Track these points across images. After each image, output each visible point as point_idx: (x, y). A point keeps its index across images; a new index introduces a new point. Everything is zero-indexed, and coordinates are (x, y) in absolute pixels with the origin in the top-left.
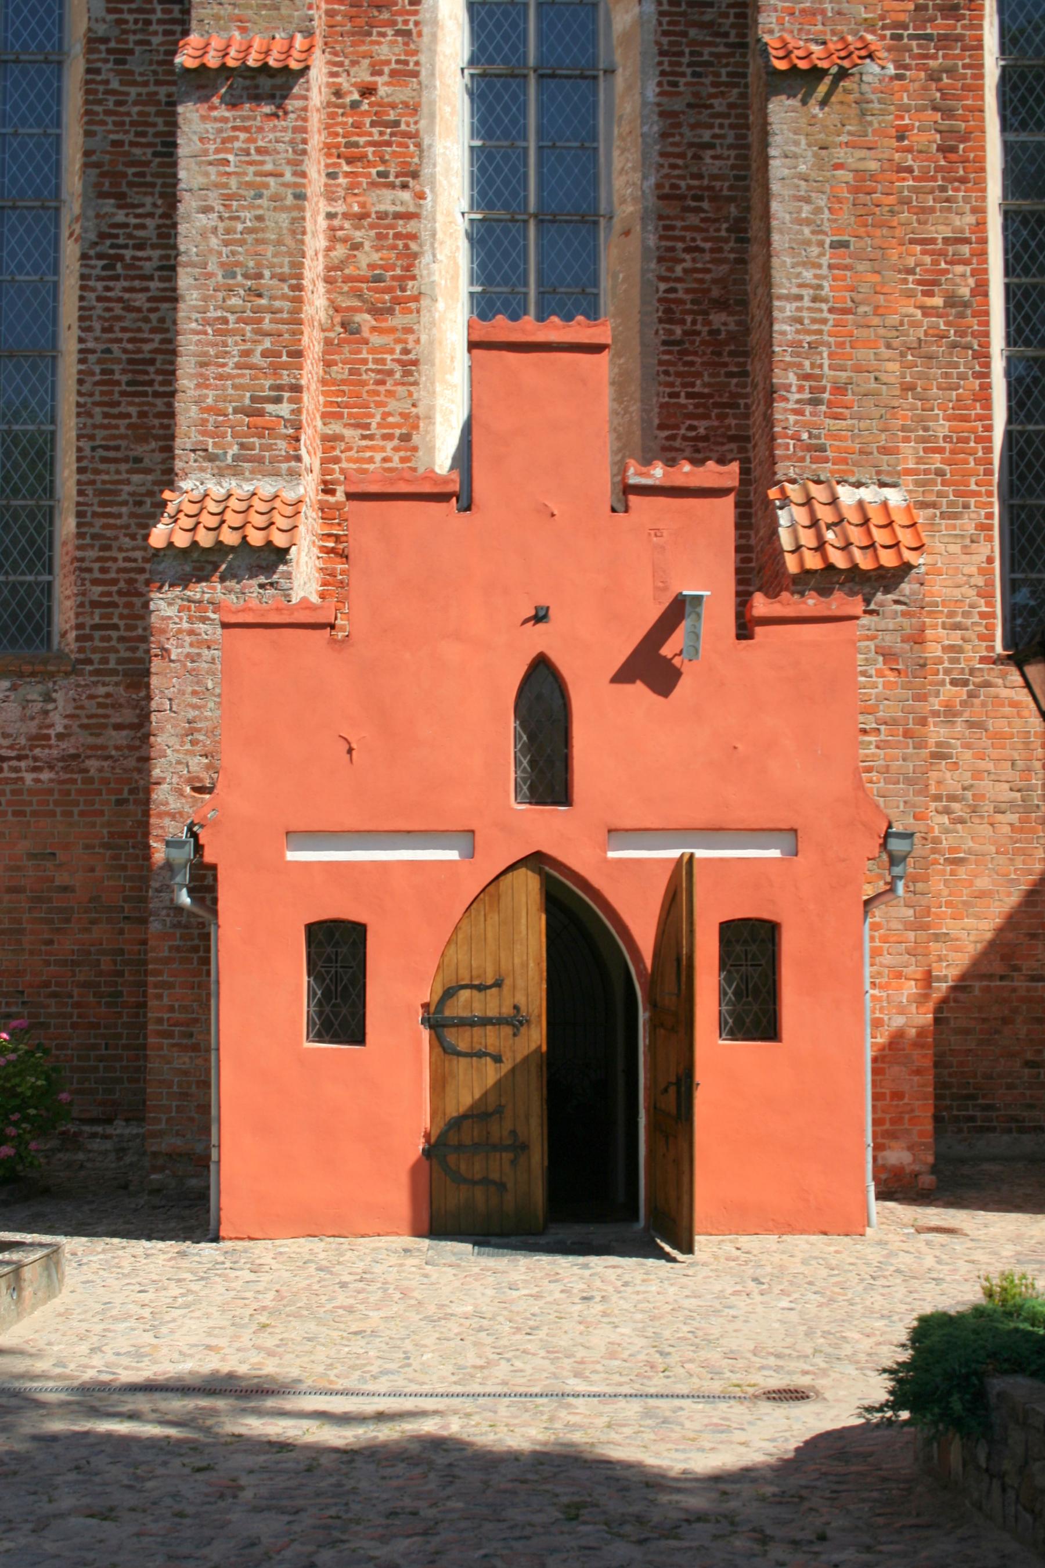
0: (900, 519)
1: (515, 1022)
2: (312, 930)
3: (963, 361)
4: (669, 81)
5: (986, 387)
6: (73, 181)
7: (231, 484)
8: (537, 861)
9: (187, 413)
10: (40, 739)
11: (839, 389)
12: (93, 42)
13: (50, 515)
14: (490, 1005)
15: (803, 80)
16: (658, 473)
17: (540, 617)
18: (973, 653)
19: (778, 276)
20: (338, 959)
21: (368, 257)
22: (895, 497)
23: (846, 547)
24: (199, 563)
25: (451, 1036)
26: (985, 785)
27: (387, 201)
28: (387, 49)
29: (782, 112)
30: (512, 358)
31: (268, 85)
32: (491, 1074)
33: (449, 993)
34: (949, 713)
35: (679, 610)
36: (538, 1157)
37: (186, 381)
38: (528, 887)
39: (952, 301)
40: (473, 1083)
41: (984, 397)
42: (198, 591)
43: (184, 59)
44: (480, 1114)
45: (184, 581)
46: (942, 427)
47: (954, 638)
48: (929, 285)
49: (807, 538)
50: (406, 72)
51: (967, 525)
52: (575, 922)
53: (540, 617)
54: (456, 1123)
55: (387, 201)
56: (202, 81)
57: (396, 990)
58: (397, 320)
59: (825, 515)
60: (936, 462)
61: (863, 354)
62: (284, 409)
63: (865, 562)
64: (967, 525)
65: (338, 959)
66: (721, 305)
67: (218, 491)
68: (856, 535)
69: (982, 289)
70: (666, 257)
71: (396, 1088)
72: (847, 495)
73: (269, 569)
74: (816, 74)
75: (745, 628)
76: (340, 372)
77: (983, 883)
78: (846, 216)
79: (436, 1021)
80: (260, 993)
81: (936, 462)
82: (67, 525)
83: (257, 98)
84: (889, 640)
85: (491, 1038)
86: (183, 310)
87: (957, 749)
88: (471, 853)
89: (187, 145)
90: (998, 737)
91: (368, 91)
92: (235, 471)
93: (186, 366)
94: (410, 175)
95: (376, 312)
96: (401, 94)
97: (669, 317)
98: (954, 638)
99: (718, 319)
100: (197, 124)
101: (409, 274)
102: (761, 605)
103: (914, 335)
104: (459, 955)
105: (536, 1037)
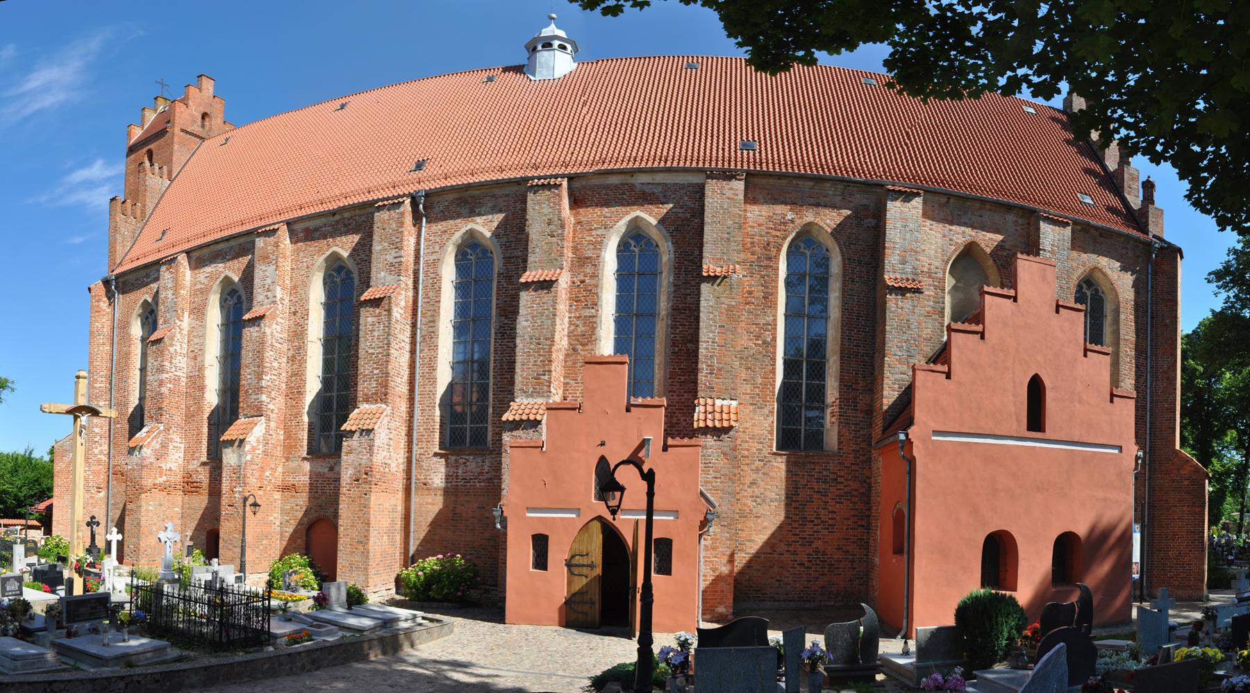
0: (732, 411)
1: (592, 566)
2: (547, 537)
3: (767, 360)
4: (677, 276)
5: (774, 369)
6: (494, 313)
7: (531, 401)
8: (600, 518)
9: (518, 379)
10: (481, 473)
11: (719, 370)
12: (499, 274)
13: (487, 407)
14: (585, 561)
15: (713, 279)
16: (640, 401)
17: (603, 444)
18: (766, 452)
19: (701, 335)
20: (541, 544)
21: (581, 329)
22: (734, 403)
23: (713, 420)
24: (516, 425)
25: (573, 569)
26: (768, 493)
27: (587, 312)
28: (589, 270)
29: (705, 287)
30: (597, 366)
31: (547, 285)
32: (584, 581)
33: (573, 557)
34: (757, 470)
35: (644, 443)
36: (597, 606)
37: (518, 370)
38: (597, 526)
39: (764, 342)
40: (580, 583)
41: (773, 372)
42: (515, 433)
43: (522, 280)
44: (581, 593)
45: (511, 430)
46: (759, 381)
47: (760, 446)
48: (758, 337)
49: (702, 417)
50: (594, 276)
51: (766, 411)
52: (612, 537)
53: (603, 444)
54: (574, 595)
55: (587, 312)
56: (527, 286)
57: (558, 555)
58: (589, 347)
59: (709, 409)
60: (757, 391)
61: (728, 359)
62: (546, 377)
63: (718, 424)
64: (766, 411)
65: (541, 544)
66: (691, 341)
67: (525, 402)
68: (717, 416)
69: (774, 339)
70: (674, 327)
71: (557, 584)
72: (718, 402)
73: (536, 426)
74: (716, 277)
75: (665, 448)
76: (570, 364)
77: (766, 524)
78: (724, 318)
79: (569, 565)
80: (518, 556)
81: (757, 391)
82: (491, 410)
83: (542, 289)
84: (726, 450)
85: (585, 571)
86: (517, 350)
87: (759, 481)
88: (579, 516)
89: (522, 303)
90: (773, 478)
91: (582, 282)
92: (532, 396)
93: (518, 366)
94: (595, 305)
95: (583, 345)
96: (593, 282)
97: (674, 345)
98: (760, 446)
99: (689, 345)
100: (525, 297)
101: (593, 333)
102: (670, 441)
103: (752, 352)
104: (576, 545)
105: (598, 571)
